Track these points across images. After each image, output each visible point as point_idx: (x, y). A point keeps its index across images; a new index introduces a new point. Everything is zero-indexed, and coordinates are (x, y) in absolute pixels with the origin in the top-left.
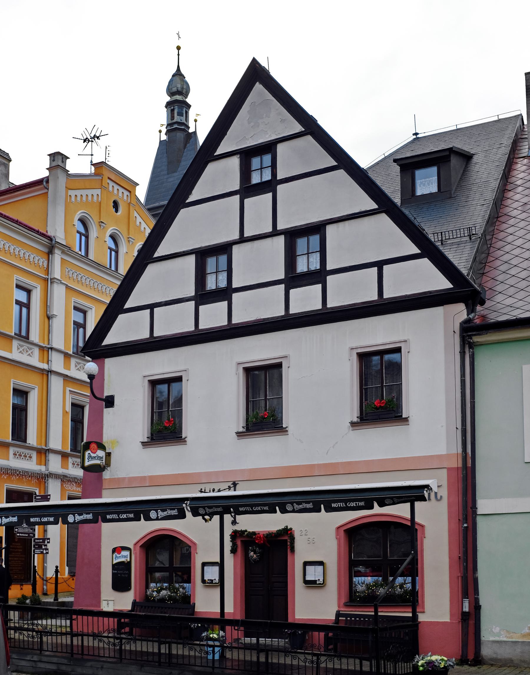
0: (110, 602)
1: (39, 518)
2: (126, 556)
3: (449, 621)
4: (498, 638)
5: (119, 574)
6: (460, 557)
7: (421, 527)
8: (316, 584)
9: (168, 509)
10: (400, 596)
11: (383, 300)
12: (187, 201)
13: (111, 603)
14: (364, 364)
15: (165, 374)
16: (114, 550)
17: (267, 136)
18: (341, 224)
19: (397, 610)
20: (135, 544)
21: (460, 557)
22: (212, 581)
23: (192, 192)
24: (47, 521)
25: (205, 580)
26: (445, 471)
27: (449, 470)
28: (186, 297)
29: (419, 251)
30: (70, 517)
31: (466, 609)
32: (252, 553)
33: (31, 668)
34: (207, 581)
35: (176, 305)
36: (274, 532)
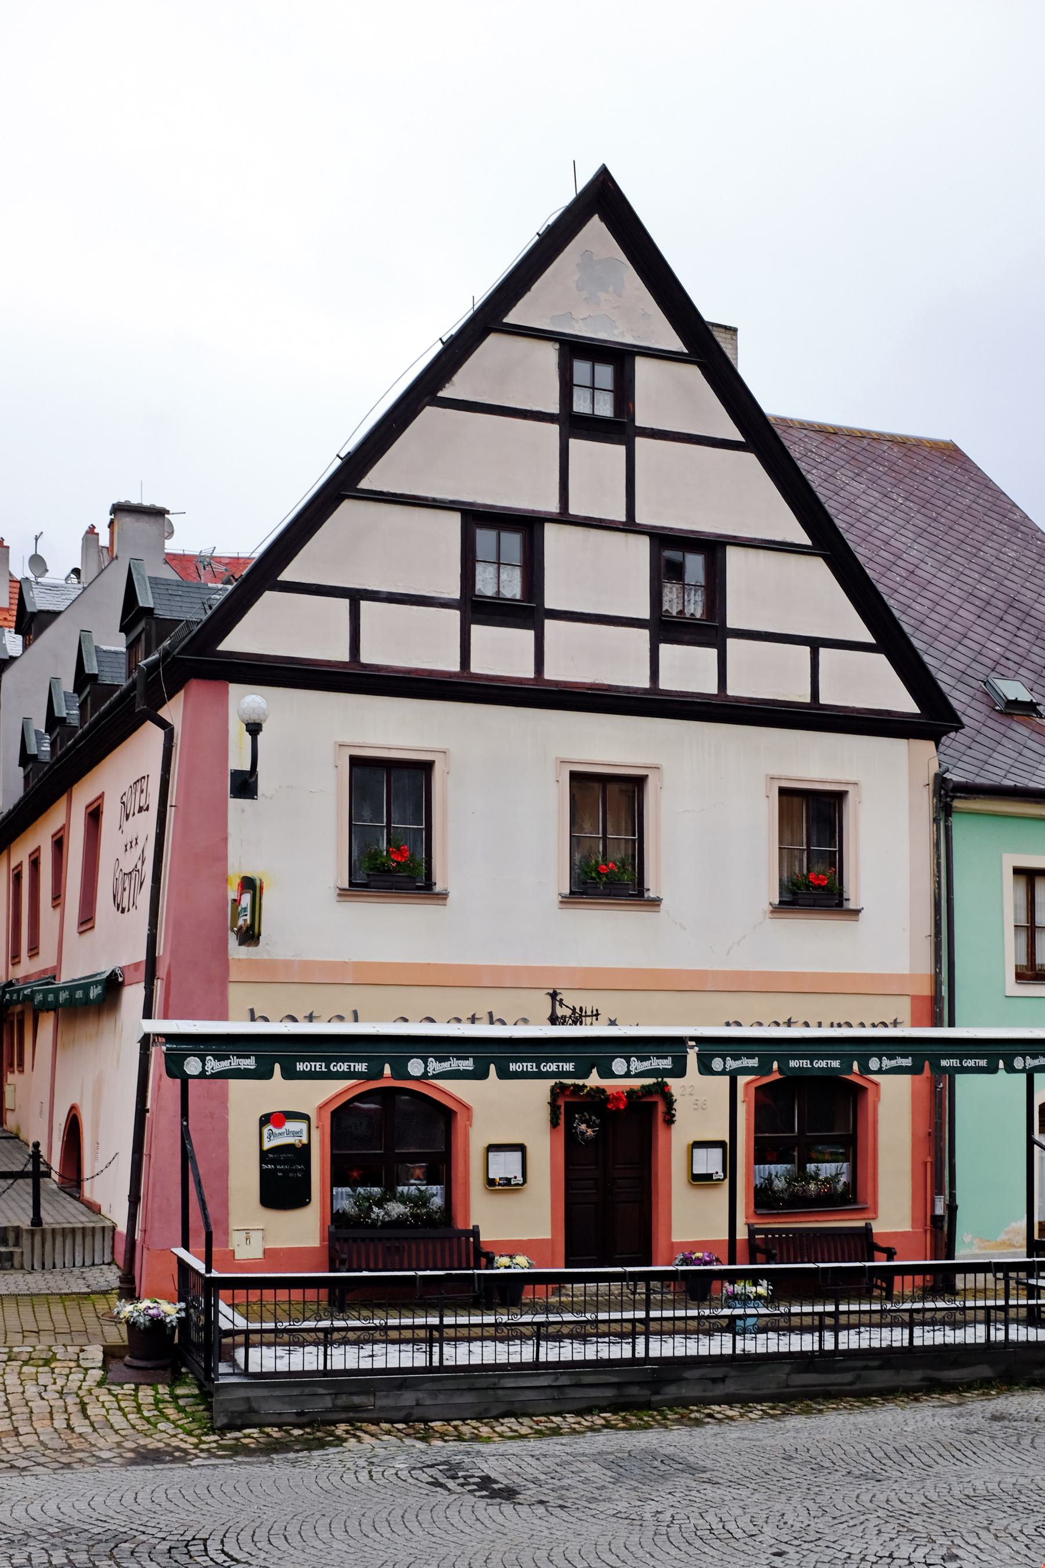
0: (252, 1234)
1: (323, 1064)
2: (298, 1133)
3: (910, 1230)
4: (969, 1250)
5: (280, 1170)
6: (930, 1133)
7: (874, 1085)
8: (712, 1180)
9: (653, 1056)
10: (819, 1196)
11: (817, 706)
12: (441, 394)
13: (256, 1237)
14: (807, 812)
15: (392, 751)
16: (265, 1120)
17: (616, 332)
18: (751, 552)
19: (829, 1218)
20: (321, 1108)
21: (930, 1133)
22: (509, 1180)
23: (453, 379)
24: (346, 1070)
25: (494, 1179)
26: (907, 1001)
27: (914, 998)
28: (439, 598)
29: (873, 641)
30: (413, 1063)
31: (940, 1210)
32: (583, 1127)
33: (550, 1401)
34: (498, 1180)
35: (415, 608)
36: (635, 1089)
